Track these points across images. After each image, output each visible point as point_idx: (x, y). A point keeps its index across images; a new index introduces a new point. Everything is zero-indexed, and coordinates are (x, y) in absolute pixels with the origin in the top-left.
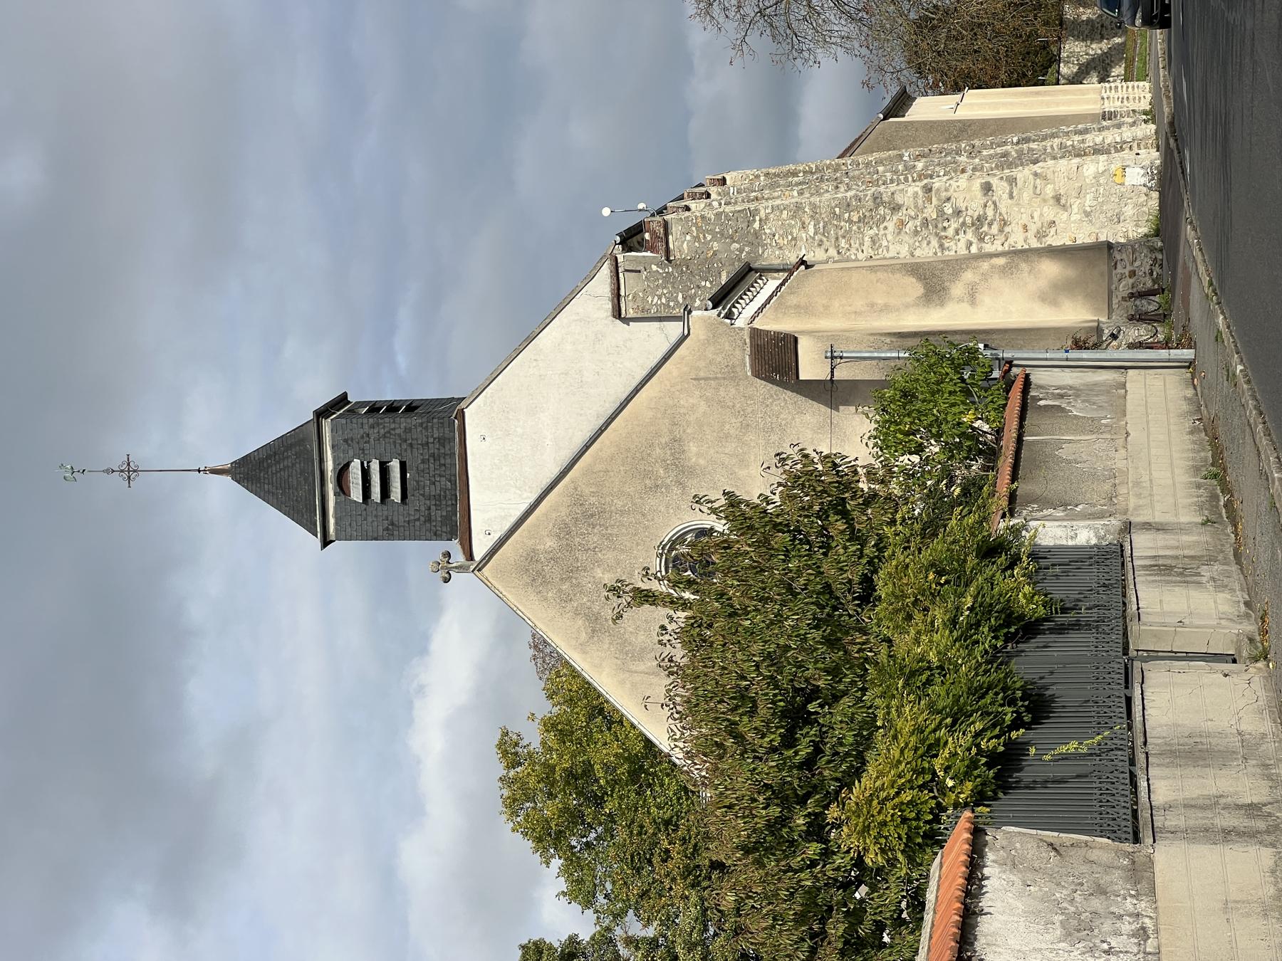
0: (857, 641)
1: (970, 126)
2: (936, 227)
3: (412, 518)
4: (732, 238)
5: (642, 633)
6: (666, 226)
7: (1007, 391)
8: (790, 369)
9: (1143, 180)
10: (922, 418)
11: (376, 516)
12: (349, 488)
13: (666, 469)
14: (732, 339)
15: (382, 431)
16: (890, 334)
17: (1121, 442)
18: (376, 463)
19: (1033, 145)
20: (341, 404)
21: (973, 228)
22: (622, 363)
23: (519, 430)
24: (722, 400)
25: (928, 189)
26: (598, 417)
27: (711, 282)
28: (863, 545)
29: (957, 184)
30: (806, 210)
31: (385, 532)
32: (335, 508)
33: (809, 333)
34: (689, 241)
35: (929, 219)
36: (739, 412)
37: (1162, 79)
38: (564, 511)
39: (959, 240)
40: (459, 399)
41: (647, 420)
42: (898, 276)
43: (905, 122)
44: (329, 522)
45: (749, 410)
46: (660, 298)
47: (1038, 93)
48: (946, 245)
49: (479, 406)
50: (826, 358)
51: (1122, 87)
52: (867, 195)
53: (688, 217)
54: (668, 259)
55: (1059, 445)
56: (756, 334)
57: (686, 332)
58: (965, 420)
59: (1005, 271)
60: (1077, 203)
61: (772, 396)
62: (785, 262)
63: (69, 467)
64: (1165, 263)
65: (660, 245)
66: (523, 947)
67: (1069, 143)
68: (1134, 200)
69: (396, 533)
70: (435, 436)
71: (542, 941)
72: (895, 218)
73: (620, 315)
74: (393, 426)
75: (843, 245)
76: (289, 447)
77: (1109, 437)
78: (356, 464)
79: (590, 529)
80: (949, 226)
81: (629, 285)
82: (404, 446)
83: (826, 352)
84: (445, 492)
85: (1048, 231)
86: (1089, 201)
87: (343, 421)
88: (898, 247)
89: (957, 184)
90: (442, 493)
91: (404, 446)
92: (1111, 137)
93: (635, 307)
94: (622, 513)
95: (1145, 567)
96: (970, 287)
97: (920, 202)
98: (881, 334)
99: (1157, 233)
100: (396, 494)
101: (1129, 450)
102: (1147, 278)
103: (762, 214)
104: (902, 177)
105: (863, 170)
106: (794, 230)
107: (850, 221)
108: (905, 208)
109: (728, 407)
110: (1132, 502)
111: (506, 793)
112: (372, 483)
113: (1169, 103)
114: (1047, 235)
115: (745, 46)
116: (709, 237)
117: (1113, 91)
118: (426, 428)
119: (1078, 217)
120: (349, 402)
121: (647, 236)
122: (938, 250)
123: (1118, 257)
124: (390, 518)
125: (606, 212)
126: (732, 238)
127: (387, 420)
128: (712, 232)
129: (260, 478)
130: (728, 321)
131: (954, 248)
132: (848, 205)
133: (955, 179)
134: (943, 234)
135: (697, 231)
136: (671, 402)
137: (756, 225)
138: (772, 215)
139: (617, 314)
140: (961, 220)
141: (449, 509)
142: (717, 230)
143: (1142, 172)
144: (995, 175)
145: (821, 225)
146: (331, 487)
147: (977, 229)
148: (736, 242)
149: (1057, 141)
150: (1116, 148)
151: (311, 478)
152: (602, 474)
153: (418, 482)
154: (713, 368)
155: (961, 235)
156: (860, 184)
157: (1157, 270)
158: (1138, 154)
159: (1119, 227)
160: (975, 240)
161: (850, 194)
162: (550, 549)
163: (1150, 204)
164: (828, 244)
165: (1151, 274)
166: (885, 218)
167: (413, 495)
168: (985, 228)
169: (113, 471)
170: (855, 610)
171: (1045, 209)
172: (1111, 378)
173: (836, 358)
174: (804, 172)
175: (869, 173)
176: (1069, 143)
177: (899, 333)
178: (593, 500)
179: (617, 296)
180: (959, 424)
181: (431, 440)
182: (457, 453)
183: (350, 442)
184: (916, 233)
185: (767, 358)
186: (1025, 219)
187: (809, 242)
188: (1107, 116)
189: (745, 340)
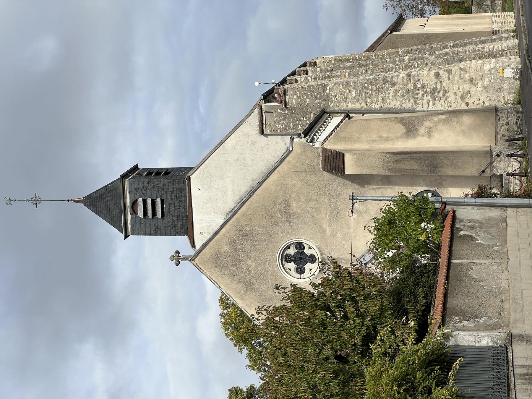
0: (358, 384)
1: (430, 36)
2: (413, 93)
3: (167, 225)
4: (316, 97)
5: (270, 291)
6: (285, 91)
7: (444, 220)
8: (341, 169)
9: (512, 75)
10: (399, 237)
11: (150, 224)
12: (137, 211)
14: (313, 152)
15: (152, 185)
16: (389, 153)
17: (504, 265)
18: (149, 200)
19: (460, 49)
20: (134, 171)
22: (264, 155)
25: (409, 75)
26: (253, 180)
27: (306, 118)
28: (363, 319)
29: (423, 73)
30: (351, 84)
31: (154, 232)
32: (131, 220)
33: (350, 151)
34: (295, 99)
35: (409, 89)
36: (316, 188)
37: (521, 22)
38: (233, 233)
39: (424, 99)
40: (190, 168)
41: (272, 191)
42: (393, 123)
43: (400, 34)
44: (128, 227)
46: (282, 125)
47: (462, 18)
48: (418, 102)
49: (197, 175)
50: (349, 199)
51: (502, 15)
52: (380, 78)
53: (295, 87)
54: (285, 107)
55: (470, 266)
56: (324, 150)
57: (291, 149)
58: (421, 238)
59: (445, 122)
61: (332, 180)
62: (341, 109)
63: (8, 198)
65: (282, 100)
66: (230, 390)
67: (477, 49)
68: (508, 81)
69: (159, 232)
70: (177, 188)
71: (238, 387)
72: (393, 89)
73: (263, 133)
74: (157, 183)
75: (368, 101)
76: (110, 192)
77: (498, 261)
78: (140, 200)
79: (245, 242)
80: (419, 93)
83: (350, 196)
84: (182, 214)
86: (486, 82)
87: (135, 180)
88: (395, 102)
89: (423, 73)
90: (181, 214)
92: (497, 46)
93: (270, 129)
94: (261, 235)
95: (522, 375)
96: (428, 129)
98: (385, 153)
99: (519, 103)
100: (159, 214)
101: (510, 272)
103: (330, 86)
104: (397, 67)
105: (380, 61)
107: (372, 90)
108: (398, 84)
110: (513, 316)
111: (223, 320)
112: (148, 209)
113: (525, 37)
116: (305, 97)
117: (498, 17)
118: (173, 184)
119: (481, 89)
120: (139, 169)
121: (276, 95)
122: (414, 104)
123: (501, 116)
124: (156, 225)
125: (257, 84)
126: (316, 97)
127: (155, 180)
129: (96, 205)
131: (421, 103)
132: (371, 83)
133: (422, 70)
134: (416, 96)
135: (300, 94)
136: (284, 183)
137: (328, 91)
139: (262, 132)
140: (425, 90)
141: (184, 221)
142: (309, 93)
143: (512, 71)
144: (441, 68)
145: (358, 91)
146: (129, 211)
147: (432, 94)
149: (471, 47)
150: (499, 53)
151: (119, 206)
153: (169, 209)
154: (304, 166)
155: (425, 97)
156: (378, 70)
158: (510, 59)
159: (501, 94)
160: (431, 100)
161: (372, 77)
162: (227, 251)
163: (516, 83)
164: (361, 100)
165: (517, 124)
166: (389, 89)
167: (167, 215)
168: (436, 94)
169: (29, 201)
170: (358, 360)
171: (465, 85)
172: (498, 214)
173: (355, 199)
174: (353, 59)
175: (382, 62)
176: (477, 49)
177: (394, 152)
178: (246, 228)
179: (262, 124)
180: (418, 240)
181: (175, 189)
182: (187, 196)
183: (137, 190)
184: (403, 96)
185: (330, 162)
186: (455, 90)
187: (352, 99)
188: (495, 32)
189: (319, 153)
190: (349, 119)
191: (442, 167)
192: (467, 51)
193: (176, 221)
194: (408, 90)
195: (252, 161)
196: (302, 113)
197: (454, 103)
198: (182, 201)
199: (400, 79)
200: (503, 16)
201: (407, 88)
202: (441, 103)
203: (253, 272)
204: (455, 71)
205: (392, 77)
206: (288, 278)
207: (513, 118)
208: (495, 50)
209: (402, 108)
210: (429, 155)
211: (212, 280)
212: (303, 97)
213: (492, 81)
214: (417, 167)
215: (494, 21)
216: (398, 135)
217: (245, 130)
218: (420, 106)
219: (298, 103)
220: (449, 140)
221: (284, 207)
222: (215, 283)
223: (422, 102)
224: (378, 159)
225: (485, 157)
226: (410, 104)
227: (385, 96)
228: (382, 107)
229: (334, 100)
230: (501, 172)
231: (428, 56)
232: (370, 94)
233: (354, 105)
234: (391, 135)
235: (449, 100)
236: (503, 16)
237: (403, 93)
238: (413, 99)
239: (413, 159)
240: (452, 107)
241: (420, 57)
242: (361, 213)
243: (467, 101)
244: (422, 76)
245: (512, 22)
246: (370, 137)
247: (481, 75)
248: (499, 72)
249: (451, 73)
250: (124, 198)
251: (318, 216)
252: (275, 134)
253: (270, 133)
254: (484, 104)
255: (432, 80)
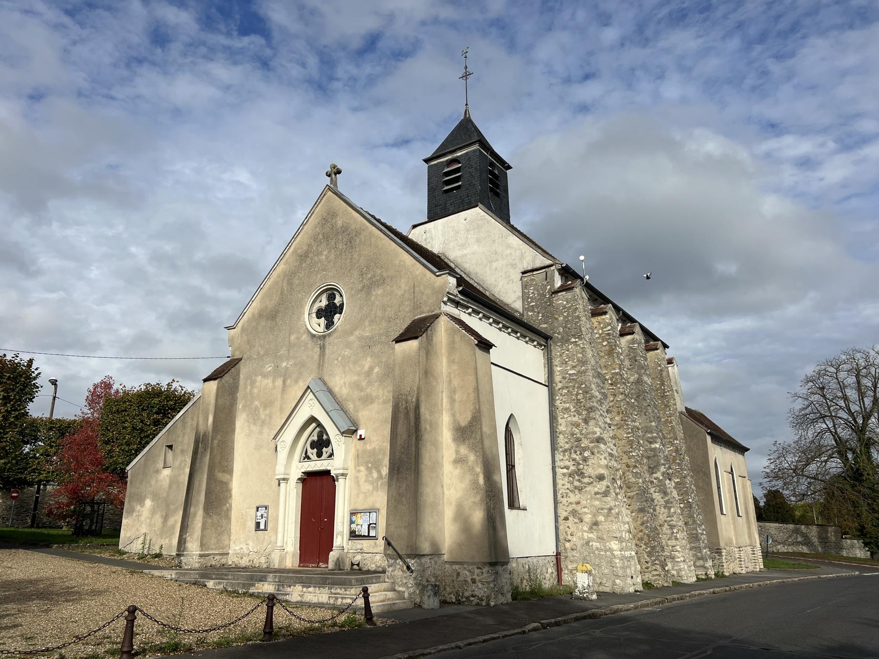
2: (577, 447)
9: (580, 585)
13: (371, 278)
15: (473, 174)
21: (576, 470)
22: (501, 280)
23: (469, 236)
24: (403, 304)
25: (599, 440)
26: (476, 273)
27: (541, 319)
29: (603, 459)
30: (583, 368)
32: (441, 162)
34: (563, 303)
35: (581, 442)
36: (397, 315)
39: (569, 461)
45: (398, 321)
46: (532, 293)
48: (566, 454)
54: (553, 293)
60: (594, 537)
64: (479, 607)
72: (580, 421)
74: (476, 178)
80: (577, 455)
81: (539, 276)
82: (467, 186)
85: (576, 517)
86: (595, 544)
88: (564, 424)
89: (603, 459)
91: (467, 186)
94: (351, 259)
96: (465, 459)
97: (590, 436)
102: (470, 593)
104: (630, 430)
106: (571, 362)
107: (577, 394)
108: (586, 427)
109: (400, 308)
114: (574, 517)
115: (797, 398)
117: (752, 552)
119: (586, 538)
122: (563, 448)
123: (484, 570)
124: (437, 188)
128: (568, 315)
130: (445, 299)
131: (565, 458)
134: (573, 451)
136: (403, 274)
137: (573, 340)
138: (579, 348)
139: (523, 273)
140: (581, 462)
142: (570, 318)
145: (575, 377)
146: (450, 157)
148: (563, 330)
152: (369, 243)
154: (420, 295)
155: (572, 463)
156: (625, 407)
157: (475, 600)
160: (570, 471)
164: (564, 383)
165: (473, 596)
168: (577, 478)
169: (466, 69)
171: (590, 516)
174: (664, 389)
175: (650, 418)
178: (358, 241)
181: (470, 198)
184: (573, 434)
186: (584, 502)
189: (434, 311)
190: (476, 345)
191: (398, 479)
192: (671, 519)
193: (441, 207)
194: (580, 441)
195: (495, 269)
196: (547, 314)
197: (567, 501)
198: (459, 207)
199: (593, 429)
200: (754, 558)
201: (583, 439)
202: (567, 484)
203: (316, 258)
204: (607, 501)
205: (594, 419)
206: (309, 299)
207: (480, 590)
208: (675, 553)
209: (558, 434)
210: (413, 460)
211: (310, 215)
212: (565, 312)
213: (596, 552)
214: (399, 443)
215: (741, 549)
216: (458, 415)
217: (527, 254)
218: (561, 457)
219: (558, 307)
220: (451, 491)
221: (377, 280)
222: (307, 219)
223: (567, 460)
224: (410, 386)
225: (407, 547)
226: (563, 443)
227: (571, 412)
228: (558, 408)
229: (562, 349)
230: (388, 572)
231: (662, 471)
232: (572, 392)
233: (558, 374)
234: (457, 405)
235: (571, 494)
236: (754, 558)
237: (576, 434)
238: (570, 448)
239: (409, 436)
240: (562, 499)
241: (660, 462)
242: (369, 376)
243: (570, 518)
244: (598, 457)
245: (742, 570)
246: (454, 377)
247: (603, 537)
248: (583, 566)
249: (604, 497)
250: (460, 149)
251: (367, 323)
252: (525, 286)
253: (524, 282)
254: (567, 541)
255: (594, 471)
